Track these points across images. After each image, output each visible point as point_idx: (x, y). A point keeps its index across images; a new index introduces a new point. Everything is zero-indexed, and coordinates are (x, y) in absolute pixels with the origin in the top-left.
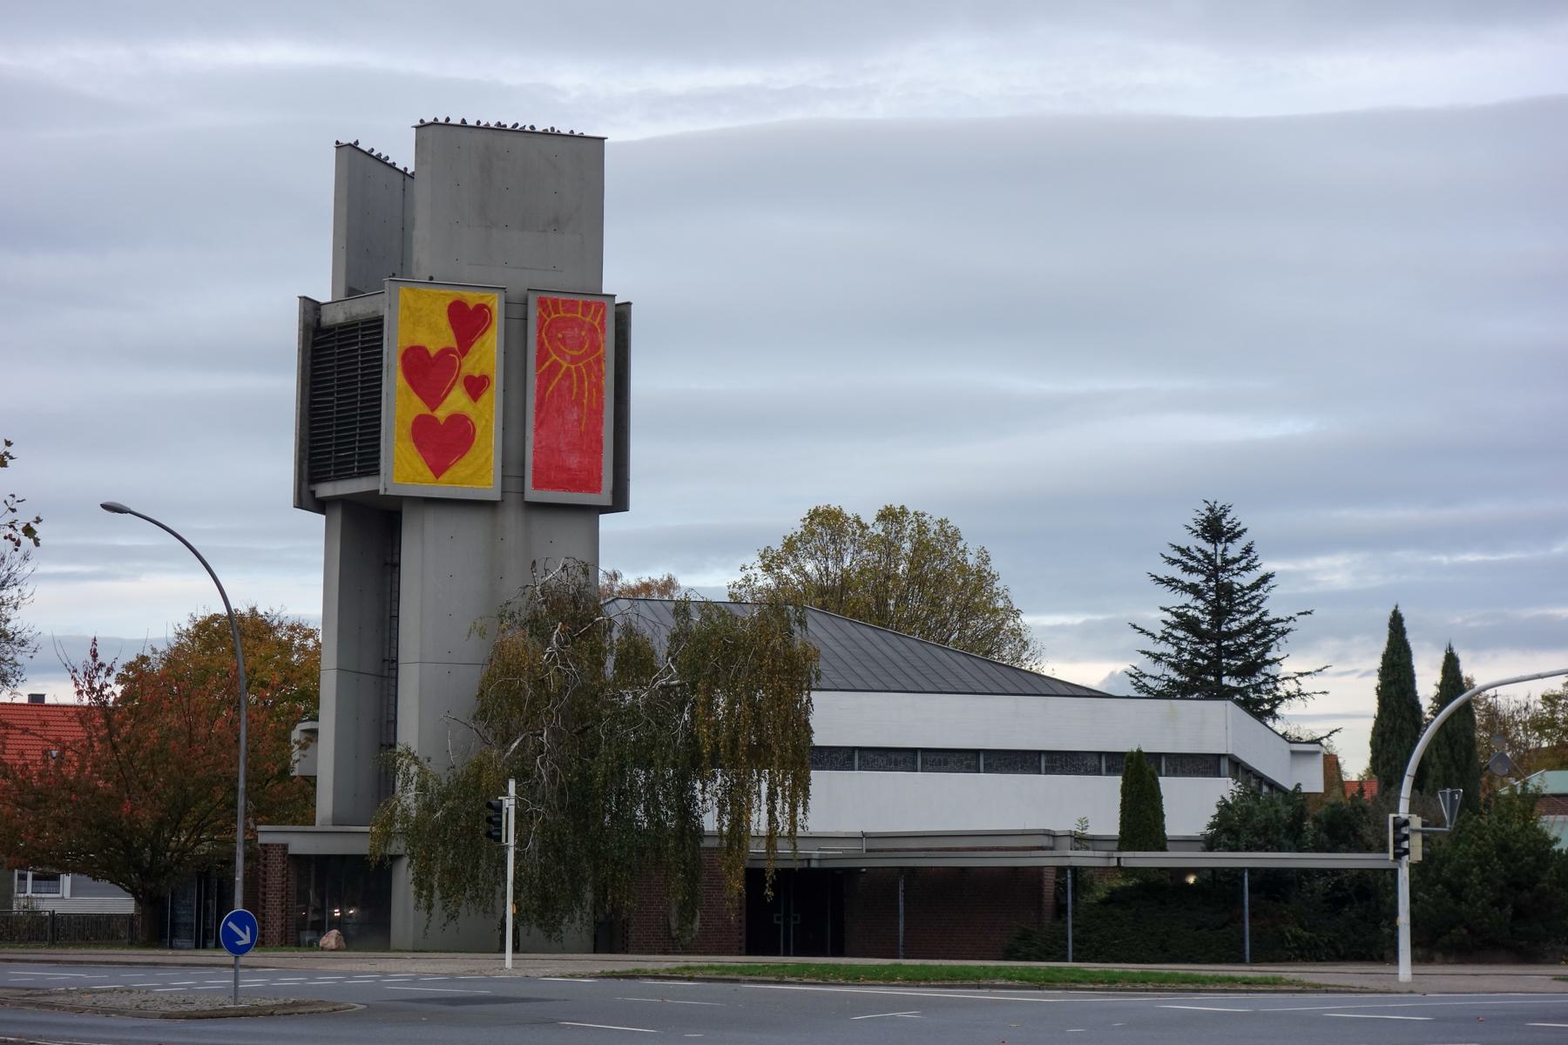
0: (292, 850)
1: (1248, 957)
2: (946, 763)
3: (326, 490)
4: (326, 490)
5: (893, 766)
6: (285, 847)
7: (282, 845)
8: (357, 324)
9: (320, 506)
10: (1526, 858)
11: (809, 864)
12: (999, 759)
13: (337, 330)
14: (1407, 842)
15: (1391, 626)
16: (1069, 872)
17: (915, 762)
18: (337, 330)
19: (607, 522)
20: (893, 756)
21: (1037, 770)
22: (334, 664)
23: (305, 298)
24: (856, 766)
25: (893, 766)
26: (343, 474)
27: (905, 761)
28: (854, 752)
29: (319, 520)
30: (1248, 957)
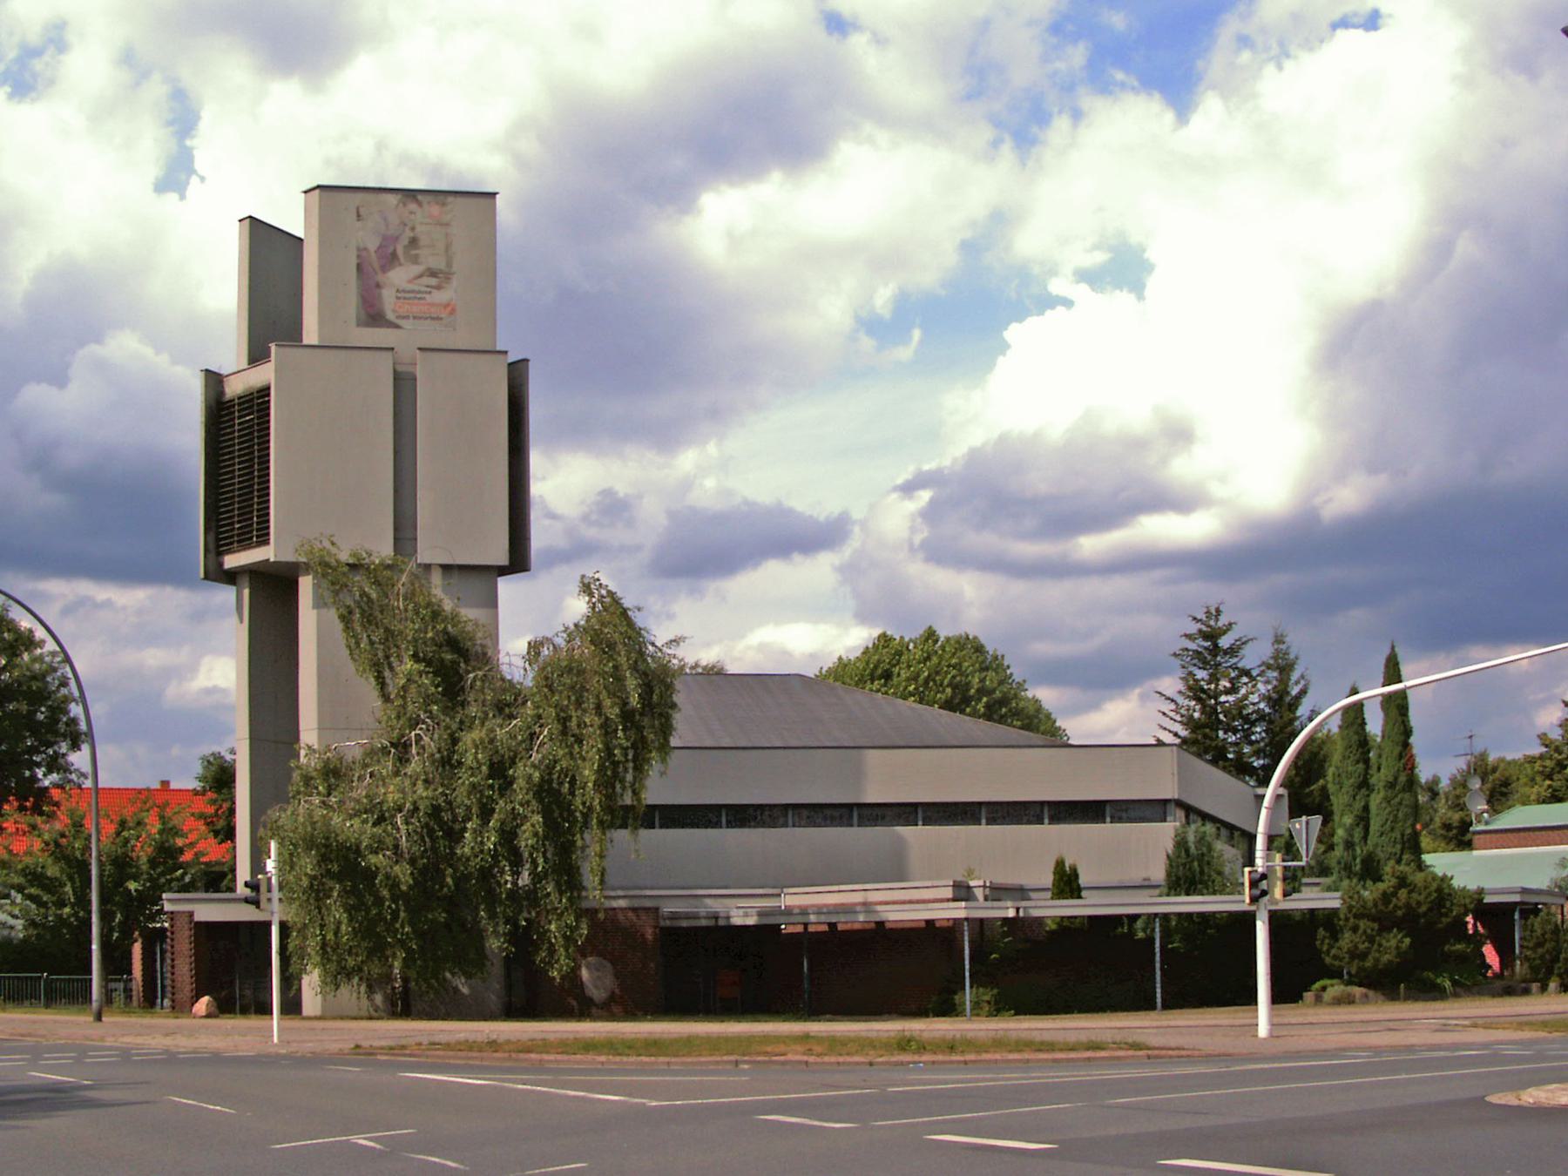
0: (198, 917)
1: (1159, 1000)
2: (883, 818)
3: (232, 561)
4: (232, 561)
5: (828, 822)
6: (191, 914)
7: (189, 912)
8: (252, 394)
9: (231, 577)
10: (450, 871)
11: (716, 921)
12: (938, 812)
13: (236, 401)
14: (1264, 882)
15: (1387, 666)
16: (966, 924)
17: (851, 817)
18: (255, 395)
19: (506, 587)
20: (828, 812)
21: (716, 825)
22: (315, 724)
23: (207, 370)
24: (790, 822)
25: (828, 822)
26: (245, 543)
27: (841, 817)
28: (980, 809)
29: (226, 595)
30: (1159, 1000)
